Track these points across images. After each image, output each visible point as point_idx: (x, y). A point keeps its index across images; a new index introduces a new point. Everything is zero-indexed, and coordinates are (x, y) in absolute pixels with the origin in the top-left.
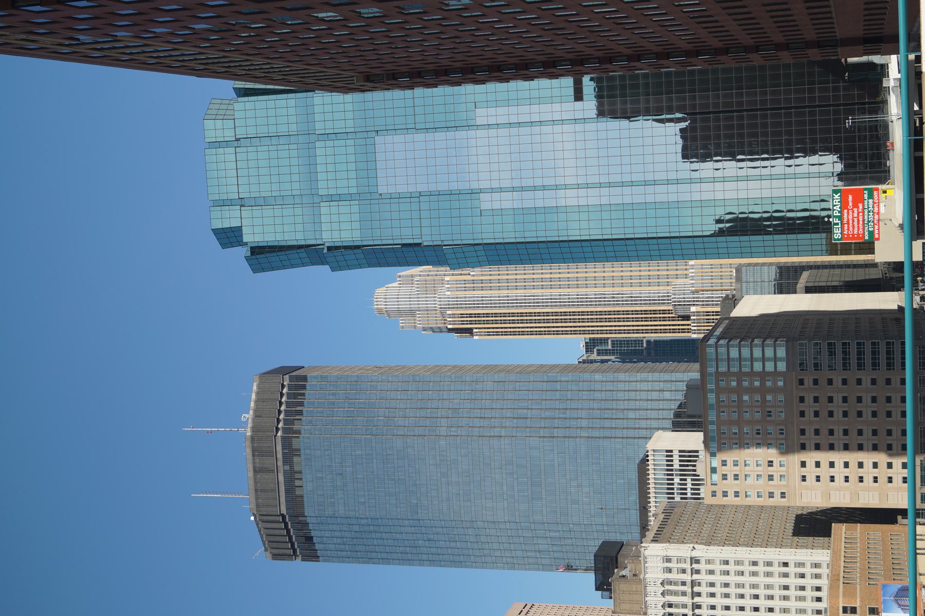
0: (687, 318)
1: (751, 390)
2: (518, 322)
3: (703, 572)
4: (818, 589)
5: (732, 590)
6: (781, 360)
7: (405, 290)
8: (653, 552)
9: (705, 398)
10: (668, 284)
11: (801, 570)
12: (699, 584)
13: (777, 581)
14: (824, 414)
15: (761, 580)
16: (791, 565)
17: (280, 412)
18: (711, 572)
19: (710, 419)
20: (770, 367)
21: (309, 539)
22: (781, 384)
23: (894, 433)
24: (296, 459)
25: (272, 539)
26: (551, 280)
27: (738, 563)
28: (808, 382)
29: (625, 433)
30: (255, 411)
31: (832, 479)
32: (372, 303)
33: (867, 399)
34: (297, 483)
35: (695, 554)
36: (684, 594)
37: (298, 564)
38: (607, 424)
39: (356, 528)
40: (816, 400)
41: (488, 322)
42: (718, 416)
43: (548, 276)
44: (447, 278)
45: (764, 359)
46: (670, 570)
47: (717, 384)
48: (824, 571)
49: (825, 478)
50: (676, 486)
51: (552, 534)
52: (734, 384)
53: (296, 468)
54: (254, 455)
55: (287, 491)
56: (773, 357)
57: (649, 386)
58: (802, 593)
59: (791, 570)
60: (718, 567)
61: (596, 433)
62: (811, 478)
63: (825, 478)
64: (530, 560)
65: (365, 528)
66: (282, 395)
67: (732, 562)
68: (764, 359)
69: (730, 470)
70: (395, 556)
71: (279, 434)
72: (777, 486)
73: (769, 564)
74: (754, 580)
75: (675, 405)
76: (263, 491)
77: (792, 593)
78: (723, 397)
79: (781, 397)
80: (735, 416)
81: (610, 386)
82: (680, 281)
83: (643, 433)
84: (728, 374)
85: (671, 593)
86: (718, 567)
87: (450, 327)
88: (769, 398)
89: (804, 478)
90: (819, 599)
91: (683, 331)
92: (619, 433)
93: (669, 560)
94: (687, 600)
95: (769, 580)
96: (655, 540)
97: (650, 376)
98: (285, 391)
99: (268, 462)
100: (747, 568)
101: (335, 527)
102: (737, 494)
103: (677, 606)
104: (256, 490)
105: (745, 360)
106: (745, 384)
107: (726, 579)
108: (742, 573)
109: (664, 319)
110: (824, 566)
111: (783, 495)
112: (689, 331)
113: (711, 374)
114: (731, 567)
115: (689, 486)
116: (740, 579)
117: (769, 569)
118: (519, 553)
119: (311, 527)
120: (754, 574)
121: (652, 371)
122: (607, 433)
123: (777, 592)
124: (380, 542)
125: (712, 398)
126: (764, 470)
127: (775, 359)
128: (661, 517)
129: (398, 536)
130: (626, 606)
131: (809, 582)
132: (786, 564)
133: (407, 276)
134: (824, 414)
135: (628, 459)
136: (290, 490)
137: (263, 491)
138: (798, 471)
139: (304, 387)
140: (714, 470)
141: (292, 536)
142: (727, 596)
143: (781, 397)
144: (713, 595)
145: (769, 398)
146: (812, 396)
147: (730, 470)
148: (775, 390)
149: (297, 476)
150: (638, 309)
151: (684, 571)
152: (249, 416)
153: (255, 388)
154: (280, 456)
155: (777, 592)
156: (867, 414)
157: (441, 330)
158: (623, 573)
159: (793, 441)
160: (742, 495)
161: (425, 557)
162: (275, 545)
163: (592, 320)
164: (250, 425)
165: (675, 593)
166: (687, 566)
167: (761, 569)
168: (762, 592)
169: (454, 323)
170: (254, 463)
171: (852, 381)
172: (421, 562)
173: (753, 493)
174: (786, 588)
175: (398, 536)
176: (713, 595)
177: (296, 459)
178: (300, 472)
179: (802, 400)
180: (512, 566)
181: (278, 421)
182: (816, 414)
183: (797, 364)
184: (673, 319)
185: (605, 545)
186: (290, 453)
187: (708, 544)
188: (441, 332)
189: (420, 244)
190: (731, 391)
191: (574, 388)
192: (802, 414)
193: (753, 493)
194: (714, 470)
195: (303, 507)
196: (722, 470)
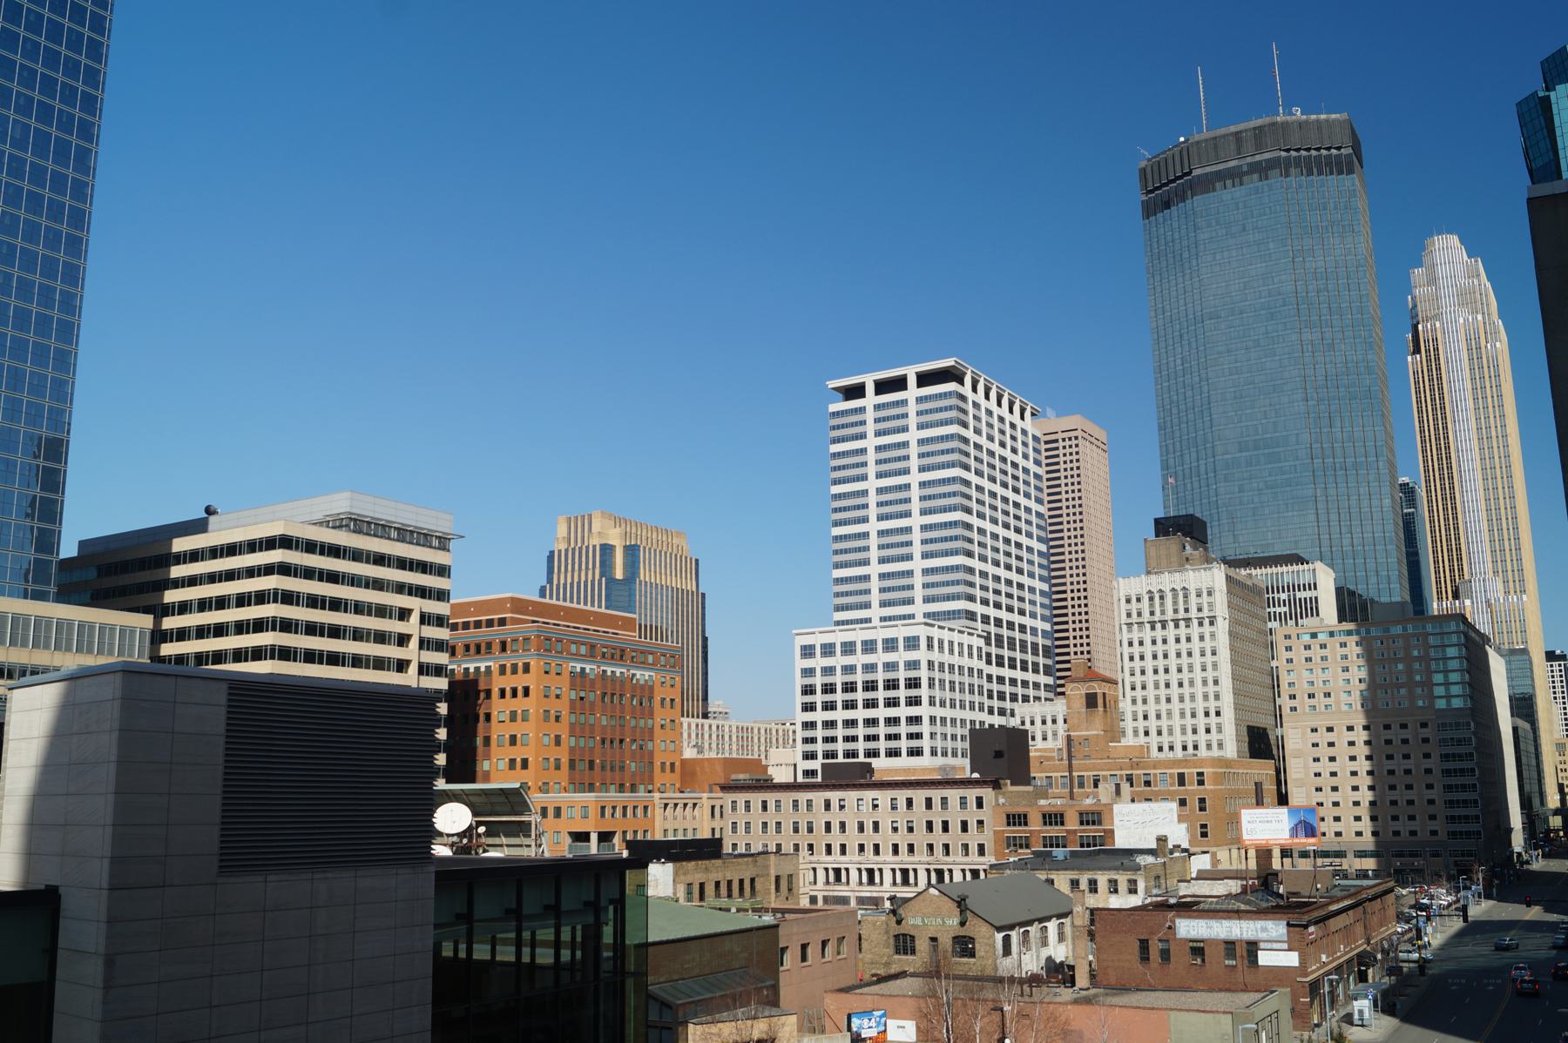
0: (1456, 596)
1: (1410, 672)
4: (1171, 748)
5: (1185, 660)
6: (1449, 702)
8: (1216, 576)
9: (1398, 622)
10: (1495, 573)
11: (1214, 729)
13: (1200, 706)
15: (1199, 690)
16: (1218, 720)
18: (1202, 638)
19: (1373, 629)
24: (1256, 176)
28: (1425, 733)
30: (1307, 122)
32: (1439, 233)
33: (1411, 795)
34: (1229, 182)
35: (1220, 620)
36: (1176, 611)
38: (1334, 517)
39: (1186, 255)
42: (1376, 638)
44: (1480, 317)
46: (1199, 595)
48: (1215, 753)
49: (1317, 752)
52: (1416, 653)
53: (1245, 178)
56: (1450, 694)
58: (1189, 731)
59: (1213, 720)
60: (1208, 644)
62: (1315, 738)
63: (1317, 752)
66: (1328, 149)
68: (1447, 684)
69: (1316, 653)
71: (1283, 154)
72: (1303, 702)
73: (1217, 697)
76: (1216, 147)
77: (1189, 721)
78: (1400, 643)
82: (1500, 586)
85: (1175, 597)
86: (1208, 644)
89: (1314, 730)
90: (1160, 749)
93: (1210, 594)
94: (1170, 615)
96: (1229, 579)
100: (1210, 675)
102: (1290, 661)
103: (1162, 604)
107: (1196, 653)
110: (1221, 753)
111: (1294, 709)
114: (1209, 658)
115: (1278, 610)
116: (1198, 668)
117: (1212, 697)
120: (1205, 682)
122: (1323, 517)
123: (1188, 705)
127: (1448, 697)
128: (1249, 583)
130: (1153, 553)
131: (1202, 737)
136: (1221, 176)
137: (1216, 147)
140: (1314, 636)
143: (1406, 704)
147: (1316, 653)
148: (1412, 697)
151: (1200, 610)
154: (1258, 158)
155: (1188, 705)
165: (1175, 603)
166: (1206, 613)
167: (1211, 689)
173: (1293, 677)
174: (1193, 715)
176: (1178, 640)
181: (1298, 150)
183: (1448, 721)
185: (1202, 525)
186: (1262, 170)
190: (1407, 649)
191: (1371, 478)
192: (1387, 727)
193: (1293, 677)
194: (1314, 636)
196: (1315, 644)
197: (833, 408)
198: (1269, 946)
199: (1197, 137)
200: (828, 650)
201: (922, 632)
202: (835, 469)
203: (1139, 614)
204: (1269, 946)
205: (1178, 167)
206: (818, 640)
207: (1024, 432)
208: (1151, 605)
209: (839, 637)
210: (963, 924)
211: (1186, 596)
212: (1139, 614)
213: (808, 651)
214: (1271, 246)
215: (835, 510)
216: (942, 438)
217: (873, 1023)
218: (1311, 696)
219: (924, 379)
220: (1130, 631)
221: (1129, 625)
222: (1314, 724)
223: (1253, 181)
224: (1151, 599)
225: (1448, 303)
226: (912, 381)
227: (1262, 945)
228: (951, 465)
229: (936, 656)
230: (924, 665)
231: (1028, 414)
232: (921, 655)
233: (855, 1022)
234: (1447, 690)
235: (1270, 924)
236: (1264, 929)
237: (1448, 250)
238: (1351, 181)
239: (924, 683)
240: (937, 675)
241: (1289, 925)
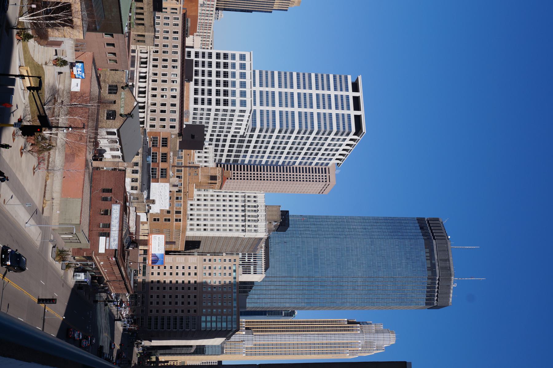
1: (217, 307)
2: (326, 327)
3: (240, 226)
4: (192, 209)
5: (228, 218)
6: (204, 322)
7: (381, 343)
8: (262, 234)
9: (238, 304)
12: (242, 220)
14: (186, 297)
17: (438, 288)
18: (237, 226)
19: (236, 294)
20: (209, 318)
21: (422, 228)
22: (204, 311)
23: (156, 288)
24: (429, 266)
25: (440, 228)
26: (310, 348)
27: (225, 230)
28: (192, 311)
29: (275, 279)
30: (450, 288)
31: (183, 268)
32: (396, 337)
34: (428, 254)
35: (244, 234)
36: (249, 216)
37: (426, 217)
38: (283, 283)
39: (400, 234)
40: (189, 303)
41: (340, 327)
42: (232, 295)
43: (312, 349)
44: (360, 349)
45: (211, 322)
46: (255, 226)
47: (232, 310)
48: (189, 227)
50: (252, 257)
51: (309, 232)
52: (225, 310)
53: (429, 261)
54: (450, 267)
55: (433, 250)
57: (264, 301)
58: (198, 217)
61: (288, 279)
62: (193, 268)
64: (318, 220)
65: (395, 234)
66: (437, 296)
67: (228, 230)
68: (211, 322)
69: (228, 271)
70: (381, 221)
71: (438, 278)
73: (212, 230)
74: (219, 223)
75: (254, 288)
76: (445, 251)
78: (230, 304)
79: (204, 304)
80: (225, 295)
81: (282, 300)
82: (250, 346)
83: (267, 279)
84: (227, 315)
86: (234, 228)
87: (358, 325)
88: (209, 304)
89: (196, 268)
90: (191, 205)
91: (249, 322)
92: (278, 279)
94: (248, 213)
95: (212, 223)
96: (261, 239)
97: (264, 305)
98: (436, 298)
101: (410, 234)
102: (225, 260)
103: (252, 211)
104: (448, 251)
105: (219, 321)
106: (220, 310)
108: (224, 225)
109: (257, 328)
110: (188, 230)
111: (205, 260)
112: (246, 322)
113: (235, 315)
114: (228, 228)
115: (246, 258)
116: (225, 223)
117: (212, 228)
118: (324, 223)
119: (421, 234)
120: (218, 225)
121: (263, 308)
122: (284, 279)
123: (209, 218)
124: (388, 228)
125: (235, 304)
126: (213, 271)
127: (206, 322)
128: (259, 247)
129: (380, 230)
130: (274, 209)
132: (205, 230)
133: (380, 350)
134: (186, 297)
135: (274, 267)
136: (432, 251)
137: (445, 251)
138: (198, 271)
139: (427, 300)
140: (235, 271)
141: (429, 230)
142: (230, 216)
143: (204, 304)
144: (237, 216)
145: (209, 304)
146: (191, 305)
147: (228, 271)
149: (429, 258)
150: (269, 333)
151: (249, 226)
152: (453, 285)
153: (451, 299)
154: (437, 267)
155: (209, 218)
156: (167, 297)
157: (363, 323)
158: (275, 223)
159: (199, 288)
160: (223, 260)
161: (367, 221)
162: (438, 225)
163: (291, 327)
164: (452, 281)
165: (252, 216)
166: (247, 228)
167: (215, 228)
168: (215, 218)
169: (357, 327)
170: (449, 264)
171: (173, 311)
172: (369, 218)
174: (205, 220)
175: (380, 230)
177: (429, 266)
178: (427, 259)
179: (195, 303)
180: (327, 217)
181: (438, 284)
182: (189, 297)
184: (253, 328)
185: (285, 231)
186: (432, 268)
187: (238, 238)
188: (363, 322)
190: (227, 307)
192: (195, 297)
194: (235, 271)
195: (425, 243)
196: (231, 271)
197: (349, 77)
198: (108, 241)
200: (243, 66)
201: (248, 108)
202: (322, 76)
203: (249, 201)
204: (108, 241)
206: (247, 62)
208: (252, 206)
210: (121, 115)
211: (255, 221)
212: (249, 201)
213: (243, 57)
214: (399, 269)
217: (79, 73)
218: (210, 268)
219: (358, 118)
220: (242, 196)
221: (244, 197)
222: (198, 268)
224: (255, 206)
226: (358, 113)
227: (108, 239)
230: (233, 108)
231: (338, 162)
232: (238, 107)
234: (214, 321)
235: (116, 242)
239: (226, 108)
241: (116, 250)
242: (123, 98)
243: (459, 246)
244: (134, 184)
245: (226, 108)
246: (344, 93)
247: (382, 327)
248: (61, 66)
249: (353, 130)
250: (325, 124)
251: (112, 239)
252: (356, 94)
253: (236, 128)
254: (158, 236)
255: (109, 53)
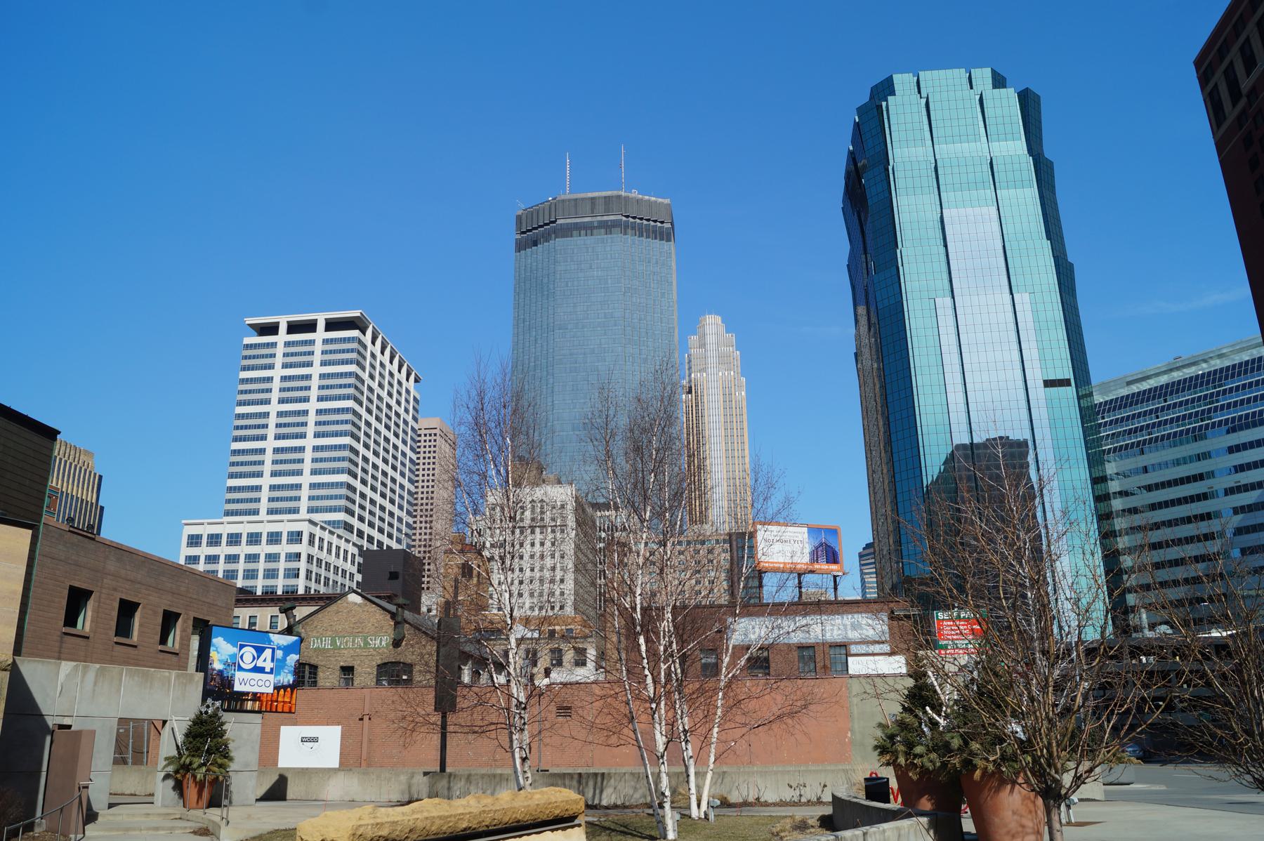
21: (535, 244)
24: (603, 231)
32: (710, 313)
39: (545, 280)
53: (595, 231)
76: (576, 206)
99: (600, 207)
136: (579, 228)
137: (576, 206)
141: (536, 231)
152: (634, 194)
154: (605, 218)
161: (521, 337)
186: (608, 227)
189: (69, 727)
197: (247, 341)
199: (563, 197)
200: (214, 540)
201: (305, 528)
202: (242, 392)
205: (547, 217)
206: (205, 531)
207: (408, 391)
209: (225, 530)
210: (397, 643)
213: (194, 541)
215: (237, 428)
216: (342, 375)
217: (266, 661)
219: (331, 325)
223: (600, 235)
225: (712, 361)
227: (854, 649)
228: (348, 397)
229: (315, 551)
230: (304, 557)
231: (412, 378)
232: (303, 548)
233: (221, 650)
236: (855, 627)
237: (713, 324)
238: (670, 247)
239: (302, 574)
240: (314, 569)
241: (892, 617)
242: (334, 642)
243: (568, 185)
244: (569, 656)
245: (302, 574)
246: (280, 350)
247: (694, 338)
248: (222, 752)
249: (355, 333)
250: (341, 386)
251: (853, 635)
252: (283, 328)
253: (345, 559)
254: (761, 545)
255: (163, 640)
